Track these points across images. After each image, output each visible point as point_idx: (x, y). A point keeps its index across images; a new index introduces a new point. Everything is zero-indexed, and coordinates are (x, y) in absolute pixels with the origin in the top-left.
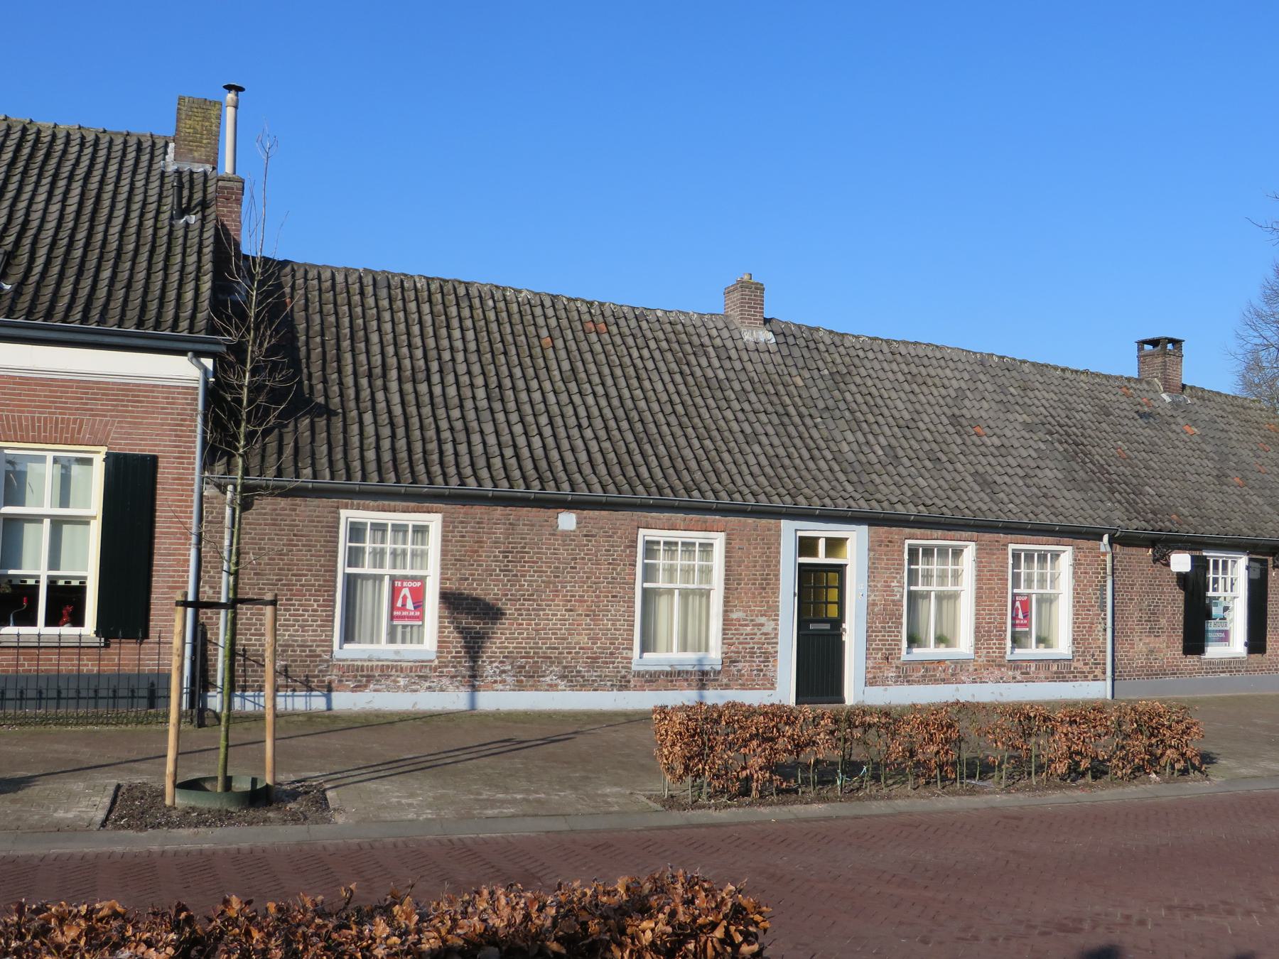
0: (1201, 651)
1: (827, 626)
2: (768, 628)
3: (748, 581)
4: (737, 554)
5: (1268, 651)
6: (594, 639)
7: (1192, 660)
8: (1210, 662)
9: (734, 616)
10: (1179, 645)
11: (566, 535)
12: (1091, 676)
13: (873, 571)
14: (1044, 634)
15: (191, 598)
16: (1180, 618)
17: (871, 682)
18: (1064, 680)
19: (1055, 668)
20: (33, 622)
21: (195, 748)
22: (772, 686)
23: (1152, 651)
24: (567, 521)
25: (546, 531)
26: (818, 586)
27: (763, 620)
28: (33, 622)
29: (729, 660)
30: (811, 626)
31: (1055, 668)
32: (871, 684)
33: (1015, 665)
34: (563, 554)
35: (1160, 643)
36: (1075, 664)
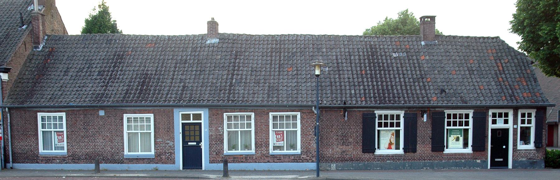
0: (414, 151)
1: (195, 143)
2: (171, 144)
3: (164, 129)
4: (158, 121)
5: (418, 152)
6: (112, 148)
7: (367, 156)
8: (448, 155)
9: (158, 140)
10: (360, 149)
11: (102, 117)
12: (310, 161)
13: (211, 124)
14: (233, 143)
15: (313, 166)
16: (360, 138)
17: (211, 162)
18: (297, 162)
19: (293, 158)
20: (201, 123)
21: (16, 133)
22: (174, 163)
23: (344, 152)
24: (102, 113)
25: (96, 116)
26: (191, 131)
27: (169, 142)
28: (201, 123)
29: (158, 155)
30: (189, 143)
31: (293, 158)
32: (212, 163)
33: (274, 156)
34: (101, 123)
35: (350, 148)
36: (303, 156)
